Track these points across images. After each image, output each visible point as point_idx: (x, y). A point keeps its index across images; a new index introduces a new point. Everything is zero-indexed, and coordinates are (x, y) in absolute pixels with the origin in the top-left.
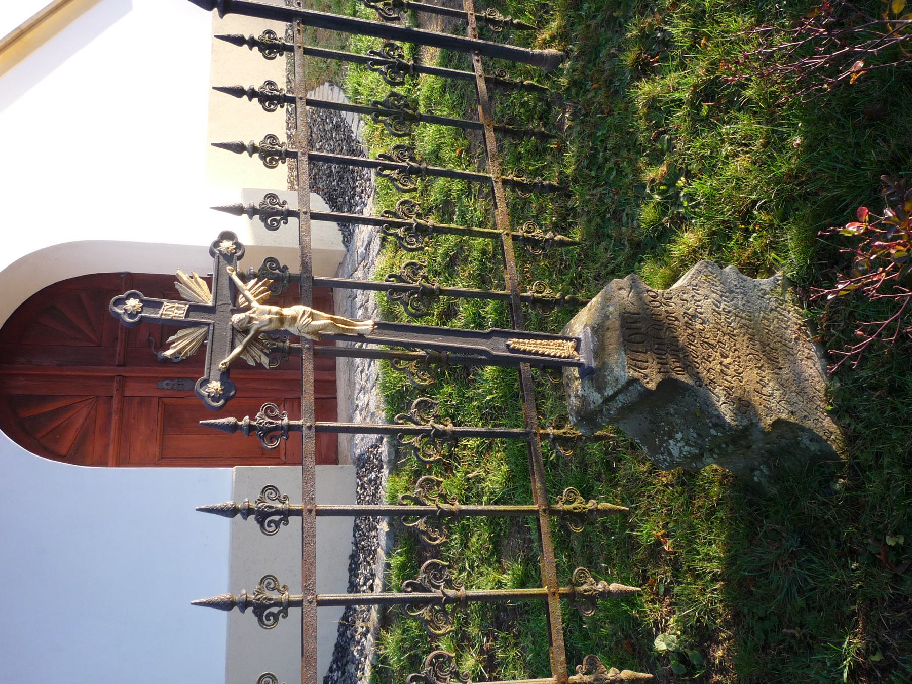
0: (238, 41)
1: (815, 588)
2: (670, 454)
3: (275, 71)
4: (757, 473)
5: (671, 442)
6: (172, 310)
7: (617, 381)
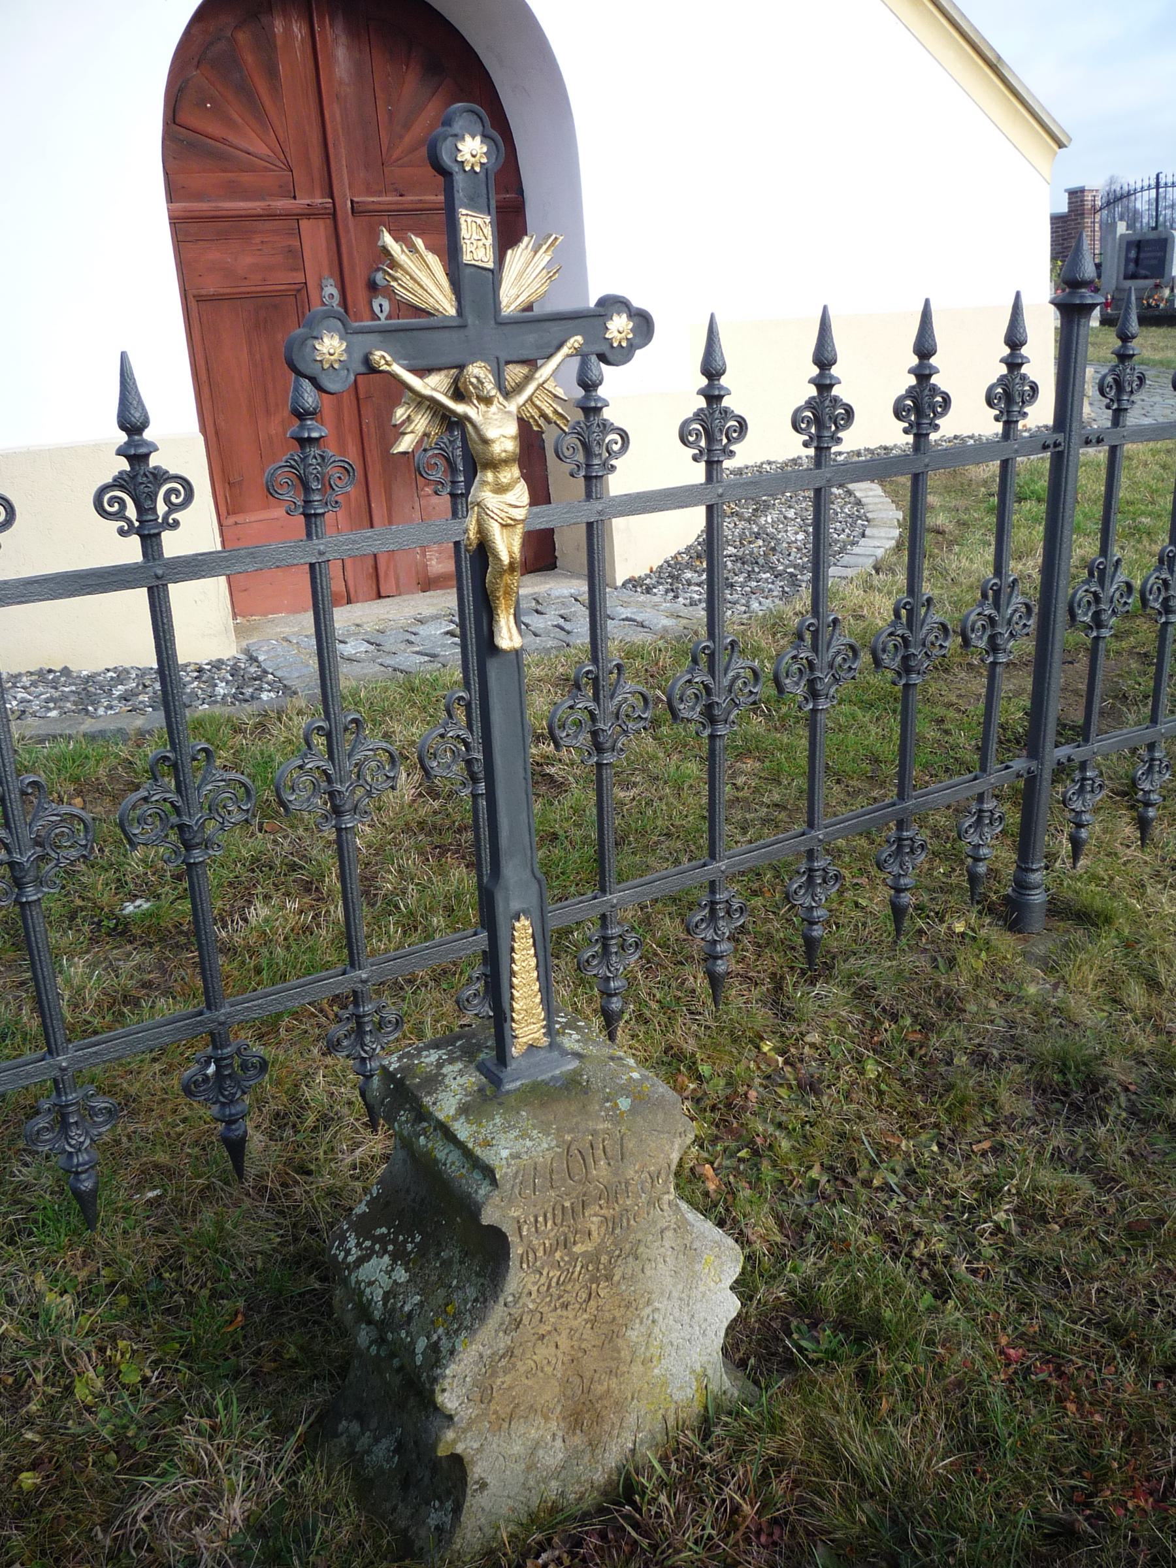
0: (1015, 339)
1: (1145, 1064)
2: (360, 1261)
3: (969, 418)
4: (355, 1427)
5: (386, 1258)
6: (476, 235)
7: (488, 1144)
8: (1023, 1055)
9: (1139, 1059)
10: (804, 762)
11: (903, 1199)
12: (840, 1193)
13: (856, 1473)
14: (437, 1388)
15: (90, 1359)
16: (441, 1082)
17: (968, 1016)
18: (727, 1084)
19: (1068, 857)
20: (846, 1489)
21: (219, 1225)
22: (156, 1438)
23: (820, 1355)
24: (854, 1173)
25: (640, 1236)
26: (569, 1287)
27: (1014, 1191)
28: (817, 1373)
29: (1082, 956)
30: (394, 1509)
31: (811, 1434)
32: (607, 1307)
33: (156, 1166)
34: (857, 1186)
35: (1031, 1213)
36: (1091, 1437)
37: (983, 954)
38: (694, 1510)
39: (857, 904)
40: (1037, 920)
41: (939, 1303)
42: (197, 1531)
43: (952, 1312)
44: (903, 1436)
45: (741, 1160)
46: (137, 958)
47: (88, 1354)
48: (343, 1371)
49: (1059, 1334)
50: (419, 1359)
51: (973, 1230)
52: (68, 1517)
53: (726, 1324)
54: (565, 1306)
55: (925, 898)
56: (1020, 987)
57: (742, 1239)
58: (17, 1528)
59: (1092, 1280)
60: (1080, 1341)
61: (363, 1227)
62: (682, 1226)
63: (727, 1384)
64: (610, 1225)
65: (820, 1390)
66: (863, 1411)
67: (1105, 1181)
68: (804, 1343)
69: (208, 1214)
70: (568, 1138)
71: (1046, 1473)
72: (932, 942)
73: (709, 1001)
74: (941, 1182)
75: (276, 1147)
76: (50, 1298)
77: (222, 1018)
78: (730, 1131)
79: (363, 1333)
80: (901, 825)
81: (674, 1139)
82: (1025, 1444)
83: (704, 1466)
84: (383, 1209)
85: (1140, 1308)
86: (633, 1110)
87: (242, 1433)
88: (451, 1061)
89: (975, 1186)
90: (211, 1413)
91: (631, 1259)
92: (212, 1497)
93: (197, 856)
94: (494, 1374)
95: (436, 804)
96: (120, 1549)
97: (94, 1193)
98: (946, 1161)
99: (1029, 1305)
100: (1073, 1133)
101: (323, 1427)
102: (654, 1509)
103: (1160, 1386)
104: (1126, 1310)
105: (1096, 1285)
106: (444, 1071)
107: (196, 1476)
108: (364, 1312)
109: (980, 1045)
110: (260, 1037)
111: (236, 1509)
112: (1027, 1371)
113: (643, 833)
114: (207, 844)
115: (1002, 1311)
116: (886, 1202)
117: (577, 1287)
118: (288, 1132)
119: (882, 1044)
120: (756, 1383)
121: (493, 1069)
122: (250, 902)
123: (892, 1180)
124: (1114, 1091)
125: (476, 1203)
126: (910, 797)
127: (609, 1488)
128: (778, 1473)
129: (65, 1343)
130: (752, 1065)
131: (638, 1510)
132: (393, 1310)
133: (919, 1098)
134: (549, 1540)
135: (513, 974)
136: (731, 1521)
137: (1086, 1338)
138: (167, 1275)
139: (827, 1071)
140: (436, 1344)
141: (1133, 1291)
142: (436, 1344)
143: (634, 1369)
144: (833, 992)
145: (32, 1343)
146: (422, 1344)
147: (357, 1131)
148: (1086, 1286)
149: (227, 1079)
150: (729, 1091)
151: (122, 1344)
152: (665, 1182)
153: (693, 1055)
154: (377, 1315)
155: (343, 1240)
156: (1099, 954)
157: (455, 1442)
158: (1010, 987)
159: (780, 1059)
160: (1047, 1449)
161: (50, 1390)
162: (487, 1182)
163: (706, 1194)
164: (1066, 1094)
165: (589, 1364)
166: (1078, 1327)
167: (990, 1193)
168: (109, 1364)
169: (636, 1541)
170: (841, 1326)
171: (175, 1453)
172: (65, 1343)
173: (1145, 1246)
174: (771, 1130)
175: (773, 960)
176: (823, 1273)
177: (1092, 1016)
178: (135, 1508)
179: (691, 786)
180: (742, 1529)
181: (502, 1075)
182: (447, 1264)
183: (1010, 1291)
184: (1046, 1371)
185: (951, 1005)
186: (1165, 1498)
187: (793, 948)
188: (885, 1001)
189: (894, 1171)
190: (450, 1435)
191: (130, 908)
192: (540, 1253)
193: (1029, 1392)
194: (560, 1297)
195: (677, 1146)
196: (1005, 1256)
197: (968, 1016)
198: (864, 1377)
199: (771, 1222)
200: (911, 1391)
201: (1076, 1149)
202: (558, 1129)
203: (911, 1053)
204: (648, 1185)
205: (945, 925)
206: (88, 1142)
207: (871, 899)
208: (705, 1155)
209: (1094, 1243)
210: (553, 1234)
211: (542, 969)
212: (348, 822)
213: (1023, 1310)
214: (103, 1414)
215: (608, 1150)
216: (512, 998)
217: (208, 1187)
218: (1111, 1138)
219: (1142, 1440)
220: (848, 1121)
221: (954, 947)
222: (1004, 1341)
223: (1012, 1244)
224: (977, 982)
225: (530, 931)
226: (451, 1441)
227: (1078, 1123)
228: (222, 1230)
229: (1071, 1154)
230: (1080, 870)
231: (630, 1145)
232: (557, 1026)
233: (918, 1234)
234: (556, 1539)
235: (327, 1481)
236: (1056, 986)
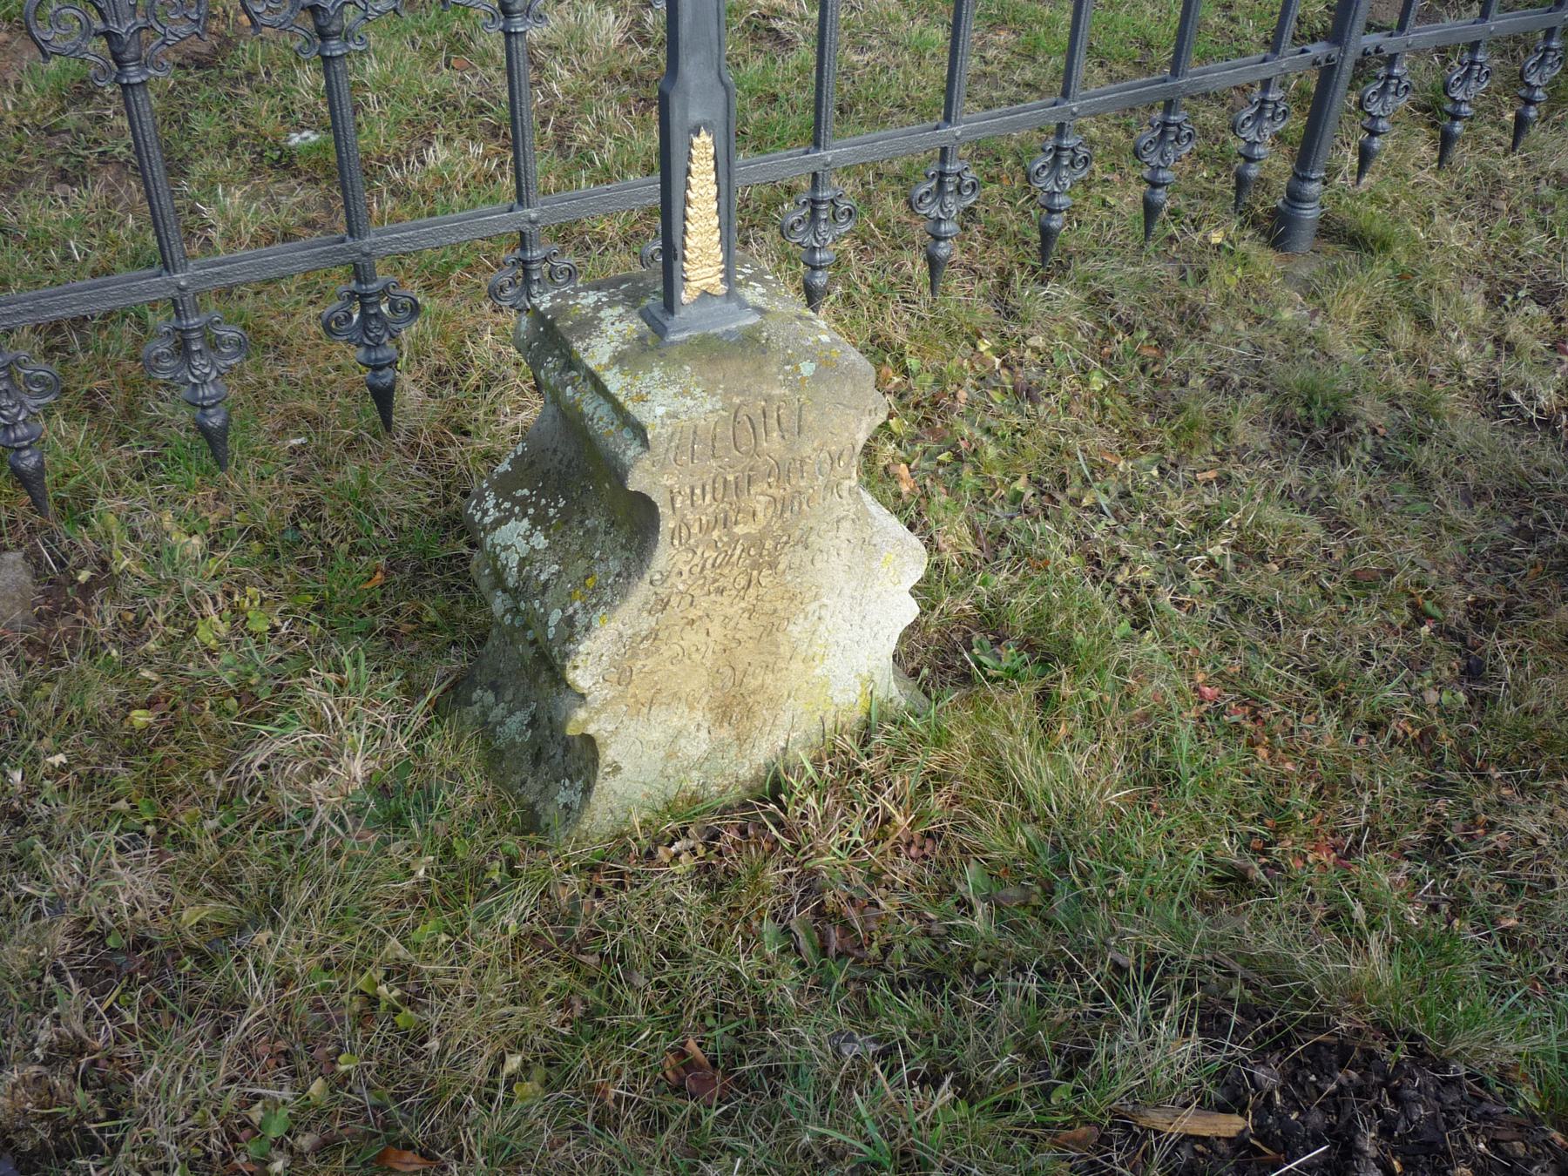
1: (1400, 408)
2: (498, 523)
4: (490, 697)
5: (526, 522)
7: (642, 399)
8: (1267, 383)
9: (1393, 401)
10: (1065, 40)
11: (1112, 522)
12: (1044, 509)
13: (1021, 796)
14: (569, 665)
15: (215, 604)
16: (597, 327)
17: (1212, 336)
18: (936, 381)
19: (1352, 172)
20: (1010, 811)
21: (363, 479)
22: (280, 688)
23: (1000, 673)
24: (1063, 489)
25: (812, 522)
26: (726, 571)
27: (1235, 525)
28: (993, 691)
29: (1351, 283)
30: (523, 783)
31: (979, 752)
32: (768, 598)
33: (301, 412)
34: (1064, 503)
35: (1250, 551)
36: (1278, 784)
37: (1239, 270)
38: (843, 815)
39: (1104, 203)
40: (1305, 238)
41: (1136, 632)
42: (316, 784)
43: (1149, 643)
44: (1078, 764)
45: (940, 463)
46: (300, 195)
47: (213, 598)
48: (482, 640)
49: (1261, 677)
50: (551, 632)
51: (1184, 561)
52: (180, 759)
53: (900, 629)
54: (721, 591)
55: (1182, 203)
56: (1274, 311)
57: (931, 545)
58: (125, 765)
59: (1305, 625)
60: (1283, 687)
61: (504, 487)
62: (862, 518)
63: (895, 692)
64: (779, 507)
65: (995, 709)
66: (1038, 734)
67: (1336, 525)
68: (984, 659)
69: (352, 468)
70: (737, 400)
71: (1226, 816)
72: (1184, 251)
73: (927, 290)
74: (1156, 507)
75: (433, 404)
76: (178, 538)
77: (367, 249)
78: (933, 432)
79: (498, 601)
80: (1169, 107)
81: (859, 413)
82: (1207, 784)
83: (859, 772)
84: (527, 468)
85: (1353, 660)
86: (816, 377)
87: (370, 691)
88: (611, 304)
89: (1193, 516)
90: (339, 670)
91: (799, 547)
92: (330, 754)
93: (335, 47)
94: (634, 656)
95: (645, 53)
96: (233, 794)
97: (224, 429)
98: (1165, 486)
99: (1233, 644)
100: (1308, 472)
101: (457, 692)
102: (800, 810)
103: (1362, 741)
104: (1337, 660)
105: (1310, 631)
106: (602, 314)
107: (319, 728)
108: (499, 580)
109: (1220, 368)
110: (428, 288)
111: (358, 768)
112: (1221, 711)
113: (873, 102)
114: (347, 35)
115: (1203, 647)
116: (1094, 523)
117: (736, 572)
118: (449, 389)
119: (1111, 356)
120: (927, 694)
121: (659, 316)
122: (430, 143)
123: (1104, 501)
124: (1360, 432)
125: (623, 465)
126: (1184, 74)
127: (755, 784)
128: (938, 787)
129: (188, 584)
130: (966, 363)
131: (784, 809)
132: (529, 577)
133: (1146, 417)
134: (685, 831)
135: (687, 202)
136: (881, 830)
137: (1290, 684)
138: (304, 526)
139: (1048, 379)
140: (571, 617)
141: (1347, 641)
142: (571, 617)
143: (793, 666)
144: (1064, 294)
145: (155, 581)
146: (556, 616)
147: (522, 394)
148: (1298, 631)
149: (367, 314)
150: (937, 389)
151: (250, 591)
152: (847, 465)
153: (902, 346)
154: (511, 582)
155: (481, 498)
156: (1371, 281)
157: (586, 722)
158: (1262, 310)
159: (998, 361)
160: (1231, 792)
161: (171, 630)
162: (638, 442)
163: (899, 495)
164: (1307, 430)
165: (743, 656)
166: (1282, 672)
167: (1208, 525)
168: (236, 610)
169: (777, 840)
170: (1027, 646)
171: (297, 705)
172: (188, 584)
173: (1369, 596)
174: (978, 434)
175: (1002, 254)
176: (1015, 589)
177: (1349, 351)
178: (251, 755)
179: (934, 55)
180: (892, 839)
181: (667, 324)
182: (591, 533)
183: (1215, 628)
184: (1241, 713)
185: (1194, 321)
186: (1348, 855)
187: (1027, 243)
188: (1122, 310)
189: (1106, 492)
190: (581, 714)
191: (296, 139)
192: (696, 529)
193: (1220, 732)
194: (715, 581)
195: (864, 425)
196: (1215, 591)
197: (1212, 336)
198: (1044, 698)
199: (965, 531)
200: (1093, 719)
201: (1309, 489)
202: (725, 390)
203: (1143, 369)
204: (827, 467)
205: (1201, 234)
206: (214, 374)
207: (1121, 198)
208: (903, 454)
209: (1314, 588)
210: (710, 510)
211: (723, 200)
212: (518, 25)
213: (1225, 649)
214: (226, 658)
215: (783, 420)
216: (685, 232)
217: (356, 439)
218: (1350, 483)
219: (1333, 794)
220: (1064, 434)
221: (1208, 259)
222: (1200, 678)
223: (1224, 580)
224: (1227, 300)
225: (712, 151)
226: (580, 721)
227: (1316, 462)
228: (365, 484)
229: (1303, 494)
230: (1362, 189)
231: (810, 417)
232: (740, 277)
233: (1124, 560)
234: (692, 830)
235: (456, 748)
236: (1314, 314)
